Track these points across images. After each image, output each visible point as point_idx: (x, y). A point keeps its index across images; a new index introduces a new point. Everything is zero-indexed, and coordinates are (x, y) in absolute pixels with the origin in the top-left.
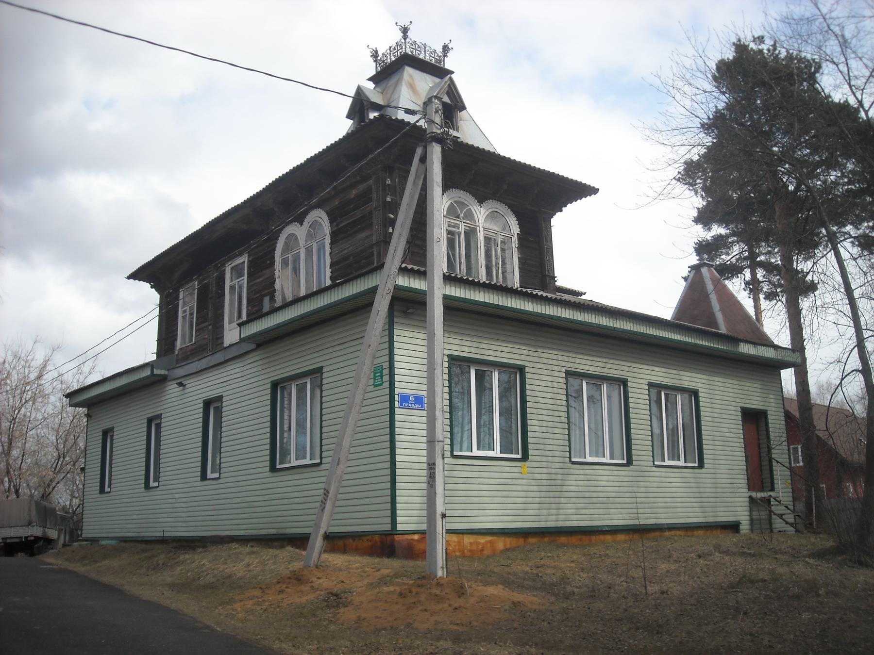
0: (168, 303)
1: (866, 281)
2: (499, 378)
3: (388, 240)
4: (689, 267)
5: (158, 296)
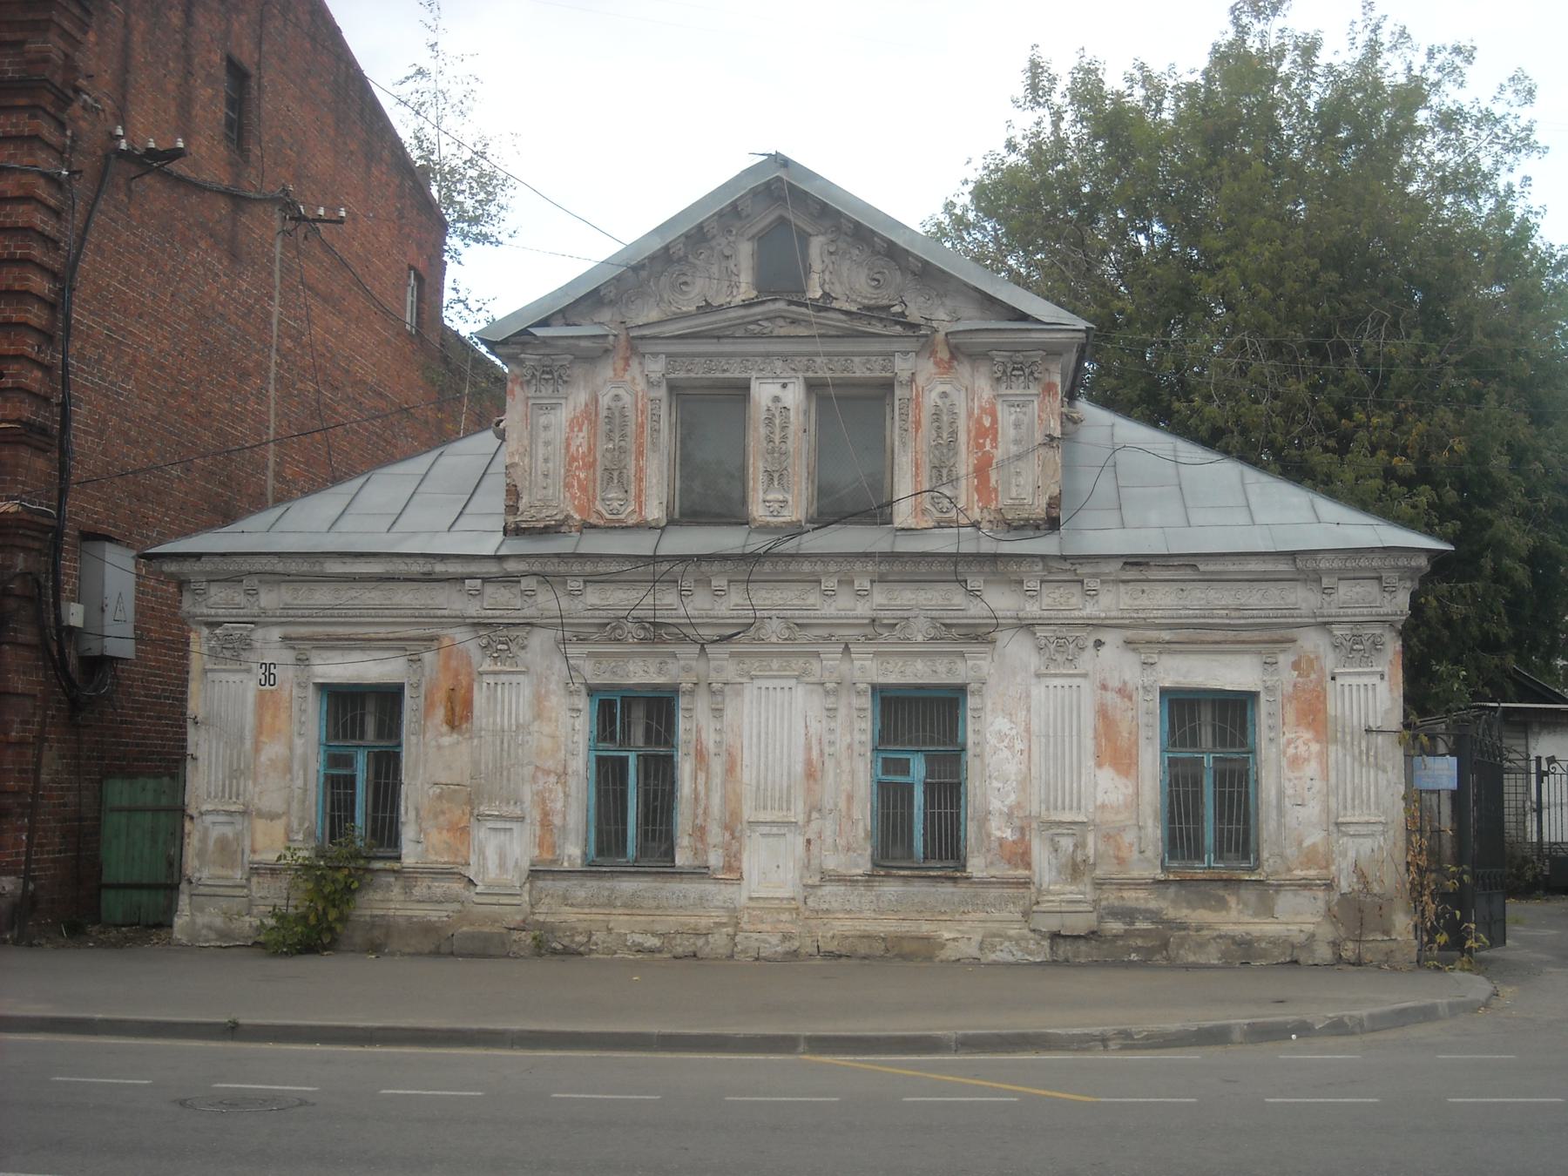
2: (952, 276)
4: (1363, 877)
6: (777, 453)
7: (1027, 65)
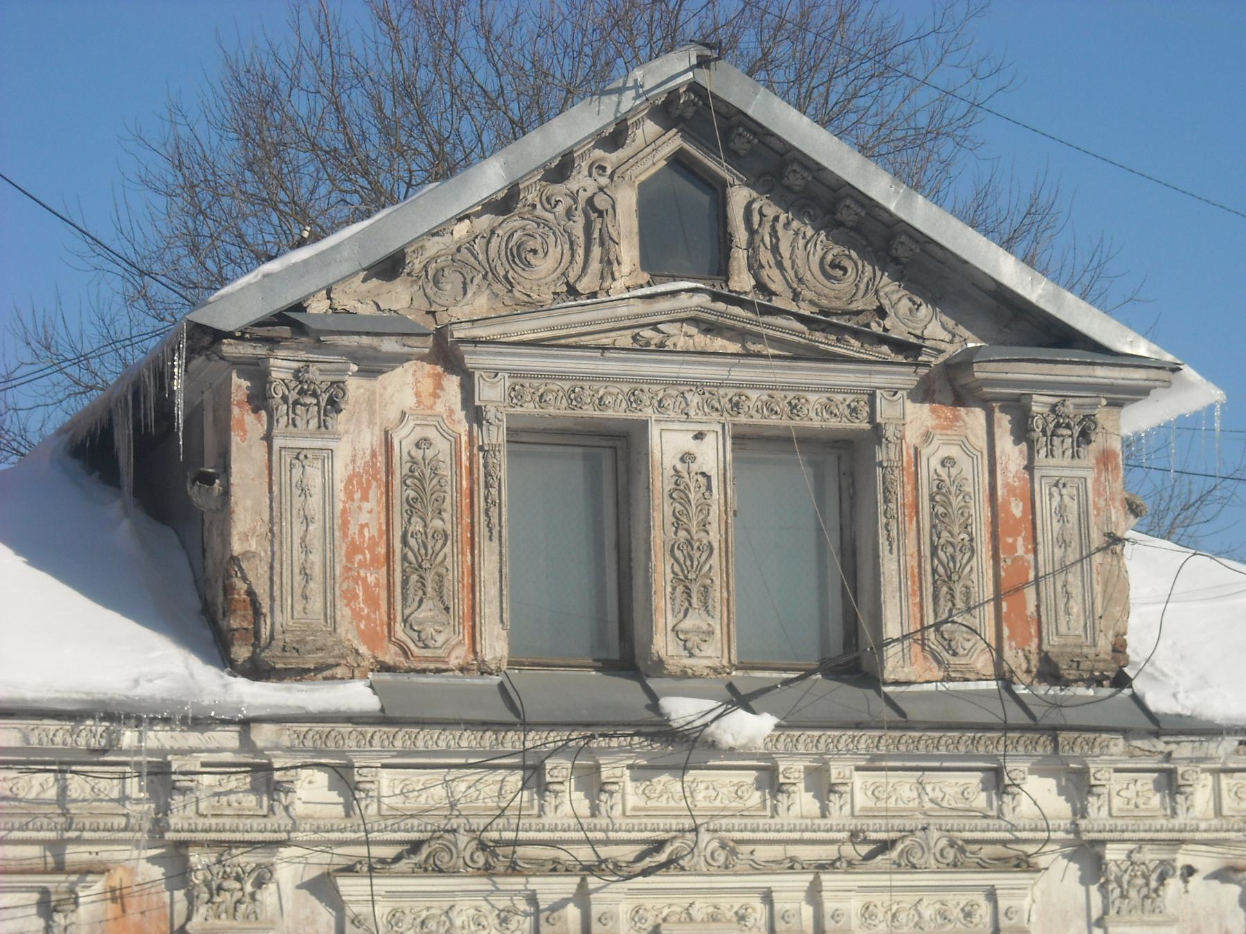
0: (241, 653)
1: (348, 92)
3: (937, 397)
5: (984, 413)
6: (915, 618)
7: (1215, 883)
